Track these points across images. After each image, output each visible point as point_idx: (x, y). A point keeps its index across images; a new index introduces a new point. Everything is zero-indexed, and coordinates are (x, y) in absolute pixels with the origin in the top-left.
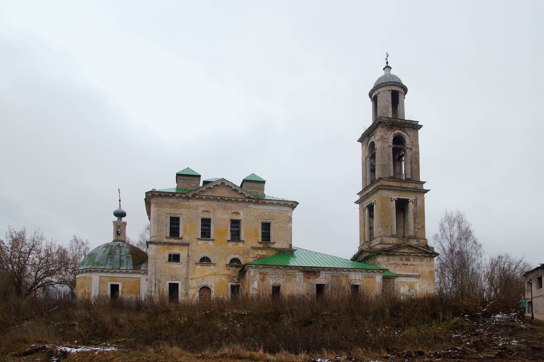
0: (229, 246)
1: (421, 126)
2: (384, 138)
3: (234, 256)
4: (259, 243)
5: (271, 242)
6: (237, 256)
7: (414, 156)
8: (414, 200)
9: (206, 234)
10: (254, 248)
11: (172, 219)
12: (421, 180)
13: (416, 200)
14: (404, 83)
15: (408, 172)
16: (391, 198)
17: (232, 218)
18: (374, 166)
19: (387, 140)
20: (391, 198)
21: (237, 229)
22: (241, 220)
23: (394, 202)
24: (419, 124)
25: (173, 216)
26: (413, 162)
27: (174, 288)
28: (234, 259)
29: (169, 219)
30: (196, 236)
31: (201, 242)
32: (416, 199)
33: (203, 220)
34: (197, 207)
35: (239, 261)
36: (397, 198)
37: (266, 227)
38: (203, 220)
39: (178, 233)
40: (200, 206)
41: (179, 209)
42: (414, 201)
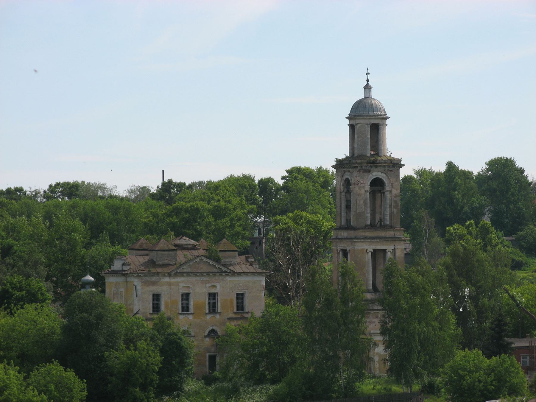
0: (207, 318)
1: (404, 165)
2: (360, 183)
3: (211, 328)
4: (235, 313)
5: (245, 311)
6: (214, 328)
7: (394, 199)
8: (392, 249)
10: (230, 319)
11: (154, 295)
13: (394, 250)
15: (387, 217)
16: (367, 250)
17: (210, 292)
18: (350, 201)
19: (363, 185)
20: (367, 250)
21: (213, 301)
22: (217, 293)
23: (370, 254)
24: (402, 163)
25: (156, 293)
26: (392, 207)
28: (211, 330)
29: (151, 296)
30: (177, 311)
31: (181, 317)
32: (395, 248)
33: (183, 295)
34: (177, 284)
35: (216, 332)
36: (373, 250)
37: (240, 296)
38: (183, 295)
39: (159, 308)
40: (180, 282)
41: (161, 287)
42: (392, 251)
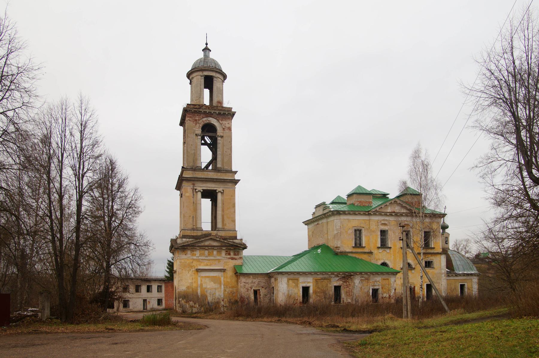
9: (384, 245)
12: (234, 169)
14: (224, 70)
27: (375, 291)
36: (202, 189)
